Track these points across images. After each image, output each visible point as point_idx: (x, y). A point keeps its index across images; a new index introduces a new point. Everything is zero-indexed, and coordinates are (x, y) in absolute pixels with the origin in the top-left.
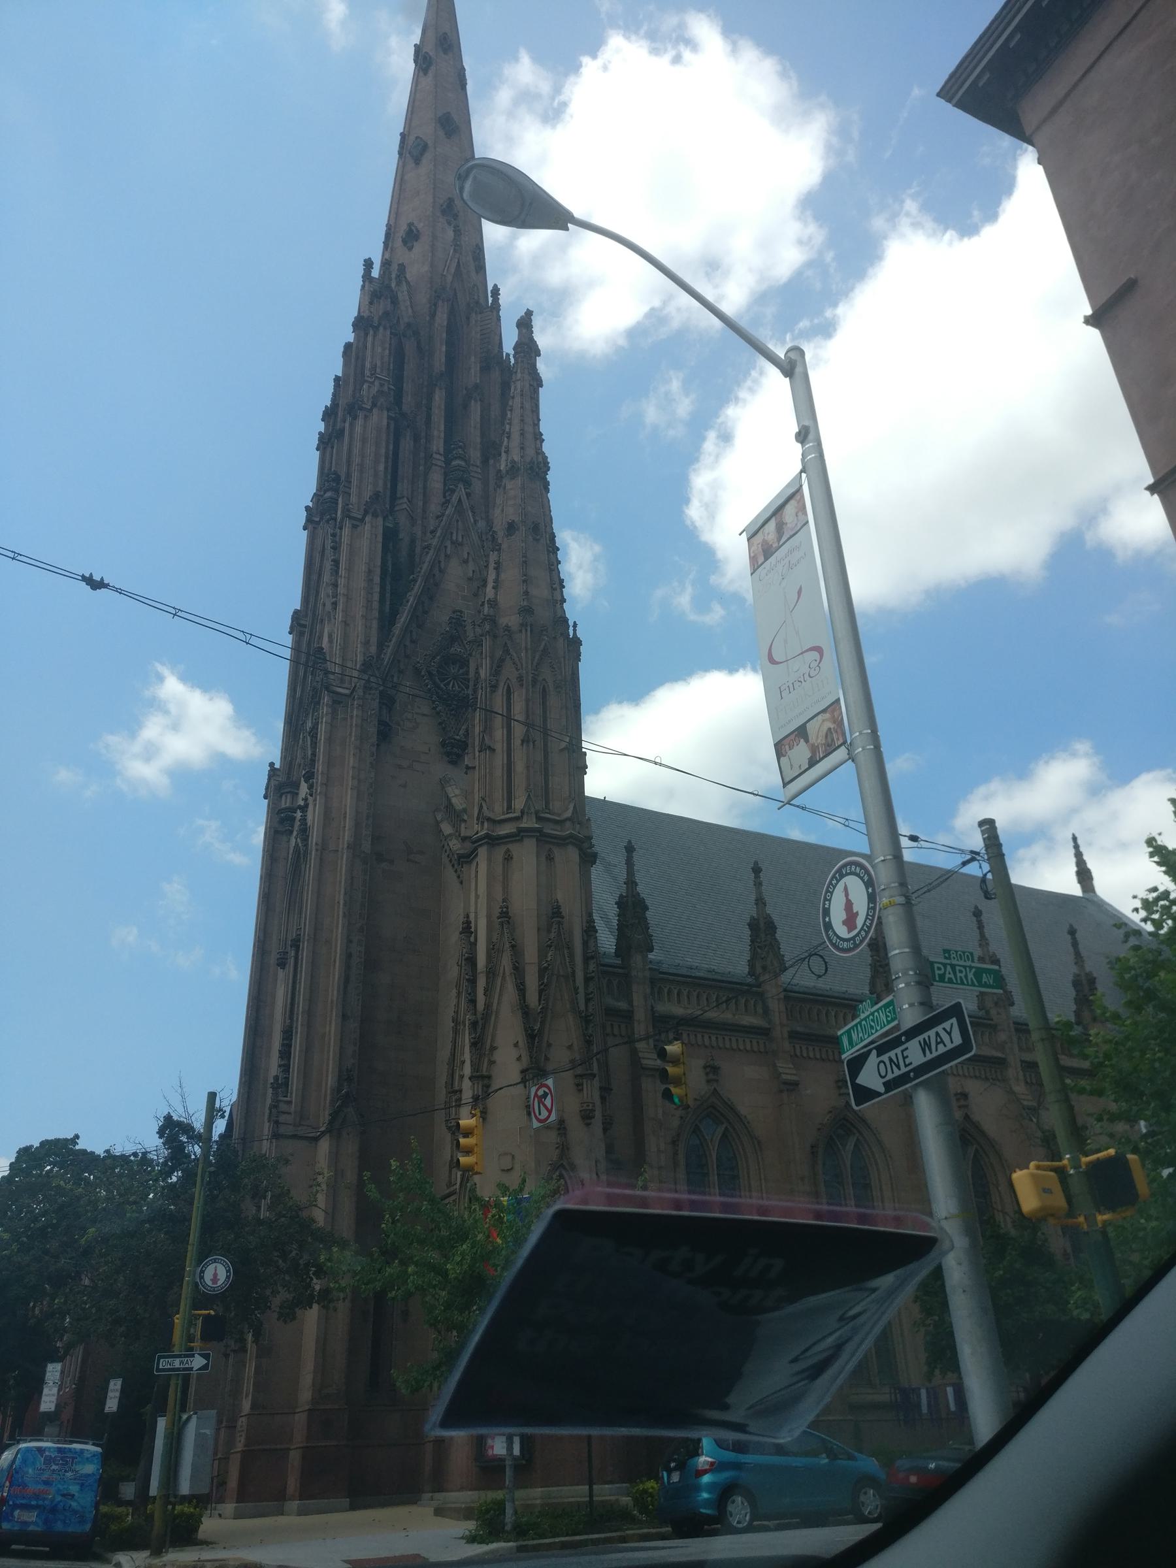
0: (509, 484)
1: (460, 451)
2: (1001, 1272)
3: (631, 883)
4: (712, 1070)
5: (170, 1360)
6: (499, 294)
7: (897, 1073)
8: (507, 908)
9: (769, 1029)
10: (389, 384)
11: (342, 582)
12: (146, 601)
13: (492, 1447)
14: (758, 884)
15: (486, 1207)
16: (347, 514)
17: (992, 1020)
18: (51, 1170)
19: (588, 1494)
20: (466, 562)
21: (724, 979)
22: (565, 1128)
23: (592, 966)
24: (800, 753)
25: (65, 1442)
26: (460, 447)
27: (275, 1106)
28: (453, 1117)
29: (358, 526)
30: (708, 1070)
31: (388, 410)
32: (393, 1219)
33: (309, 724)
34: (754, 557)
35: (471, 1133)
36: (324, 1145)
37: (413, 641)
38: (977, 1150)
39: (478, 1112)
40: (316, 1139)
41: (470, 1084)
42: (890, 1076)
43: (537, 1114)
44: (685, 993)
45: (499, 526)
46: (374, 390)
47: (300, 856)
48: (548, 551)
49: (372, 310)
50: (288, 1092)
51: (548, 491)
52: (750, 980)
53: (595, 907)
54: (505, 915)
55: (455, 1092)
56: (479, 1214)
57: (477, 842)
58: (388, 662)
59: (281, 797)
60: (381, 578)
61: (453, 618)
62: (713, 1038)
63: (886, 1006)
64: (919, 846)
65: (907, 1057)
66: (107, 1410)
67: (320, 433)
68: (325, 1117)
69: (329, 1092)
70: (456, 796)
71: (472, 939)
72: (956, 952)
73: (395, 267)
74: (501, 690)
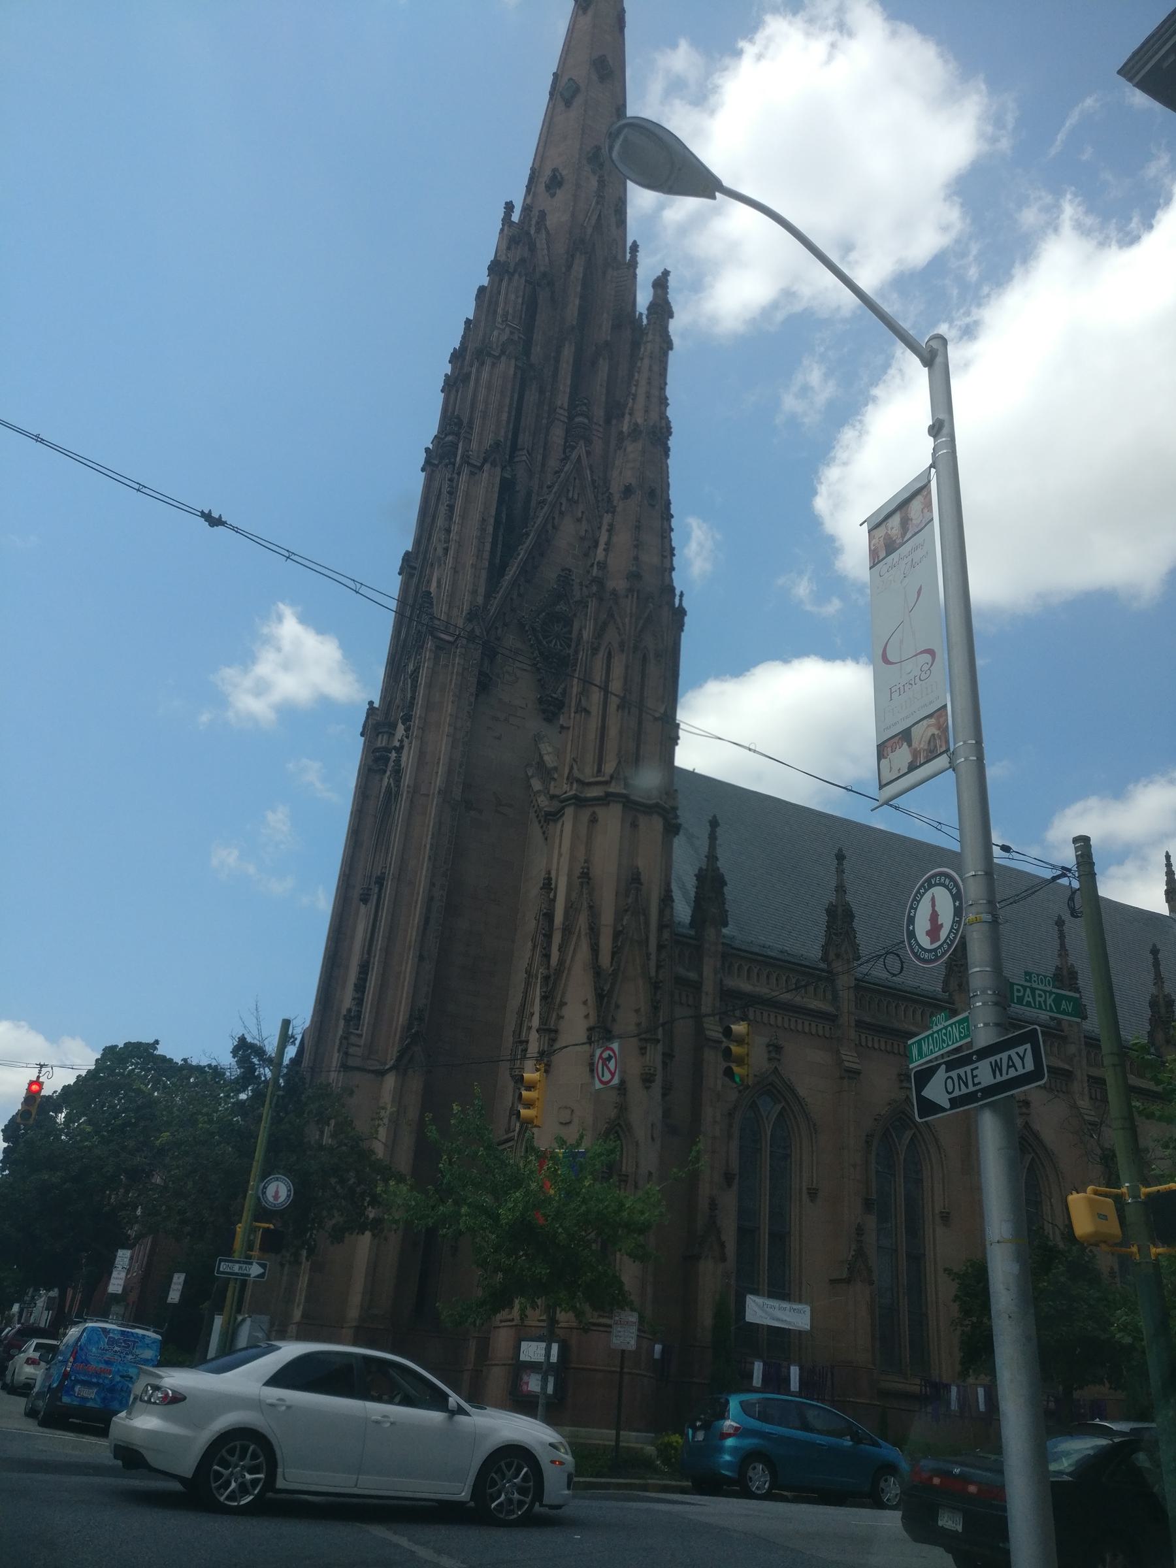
0: (630, 447)
1: (584, 408)
2: (1045, 1284)
3: (712, 857)
4: (775, 1049)
5: (230, 1264)
6: (638, 251)
7: (964, 1091)
8: (588, 869)
9: (837, 1015)
10: (520, 333)
11: (455, 528)
12: (259, 540)
13: (527, 1383)
14: (840, 871)
15: (542, 1157)
16: (466, 460)
17: (1062, 1031)
18: (133, 1070)
19: (614, 1438)
20: (579, 520)
21: (796, 961)
22: (625, 1089)
23: (666, 935)
24: (902, 756)
25: (127, 1326)
26: (585, 404)
27: (345, 1037)
28: (517, 1066)
29: (476, 473)
30: (771, 1048)
31: (517, 359)
32: (450, 1161)
33: (411, 667)
34: (874, 550)
35: (533, 1087)
36: (390, 1081)
37: (520, 595)
38: (1033, 1159)
39: (542, 1067)
40: (381, 1073)
41: (537, 1036)
42: (957, 1093)
44: (756, 970)
45: (616, 488)
46: (504, 337)
47: (391, 796)
48: (662, 517)
49: (509, 256)
50: (359, 1026)
51: (667, 455)
52: (823, 966)
53: (673, 876)
54: (586, 876)
55: (521, 1042)
56: (535, 1164)
57: (565, 801)
58: (494, 614)
59: (377, 735)
60: (494, 529)
61: (562, 576)
62: (779, 1019)
63: (960, 1022)
64: (1011, 857)
65: (976, 1076)
66: (169, 1300)
67: (446, 375)
68: (393, 1053)
69: (399, 1030)
70: (549, 754)
71: (552, 896)
72: (1038, 975)
73: (535, 213)
74: (601, 654)
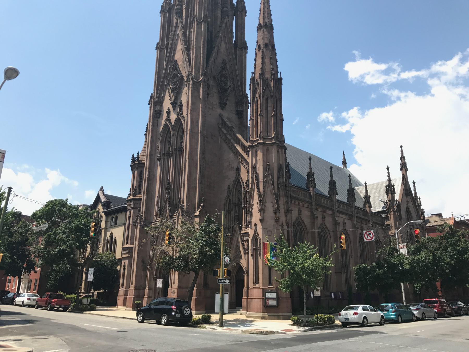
13: (268, 303)
43: (367, 238)
